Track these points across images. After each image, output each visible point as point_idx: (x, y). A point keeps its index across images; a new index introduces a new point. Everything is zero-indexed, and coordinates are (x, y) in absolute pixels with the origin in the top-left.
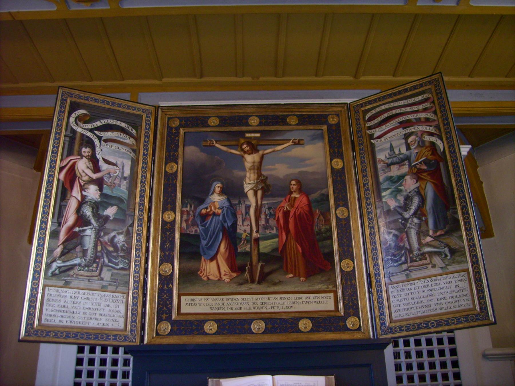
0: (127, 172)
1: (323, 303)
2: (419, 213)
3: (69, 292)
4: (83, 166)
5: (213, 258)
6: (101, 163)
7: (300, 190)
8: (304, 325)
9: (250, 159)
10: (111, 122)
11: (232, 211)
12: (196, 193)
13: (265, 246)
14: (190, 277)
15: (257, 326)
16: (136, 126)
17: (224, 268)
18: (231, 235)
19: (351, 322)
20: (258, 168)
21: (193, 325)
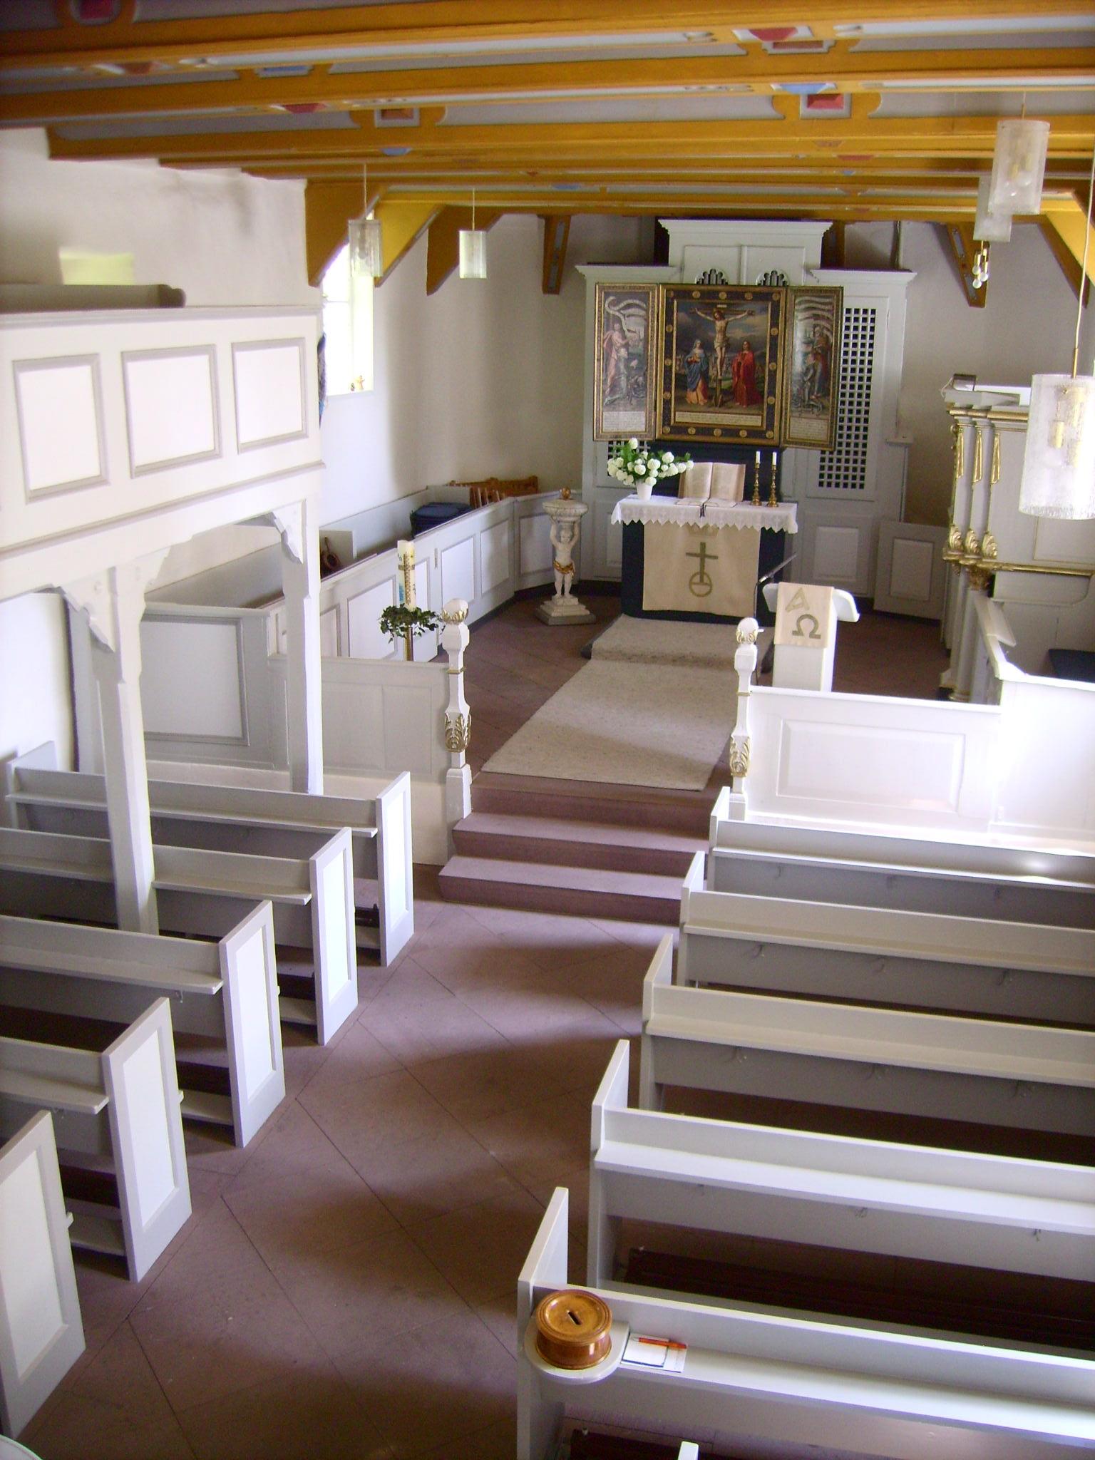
0: (642, 336)
1: (755, 421)
2: (812, 380)
3: (615, 413)
4: (616, 337)
5: (695, 390)
6: (627, 333)
7: (749, 348)
8: (743, 433)
9: (719, 324)
10: (630, 301)
11: (706, 360)
12: (685, 347)
13: (725, 384)
14: (681, 400)
15: (717, 432)
16: (646, 300)
17: (701, 396)
18: (705, 376)
19: (769, 434)
20: (724, 331)
21: (681, 428)
